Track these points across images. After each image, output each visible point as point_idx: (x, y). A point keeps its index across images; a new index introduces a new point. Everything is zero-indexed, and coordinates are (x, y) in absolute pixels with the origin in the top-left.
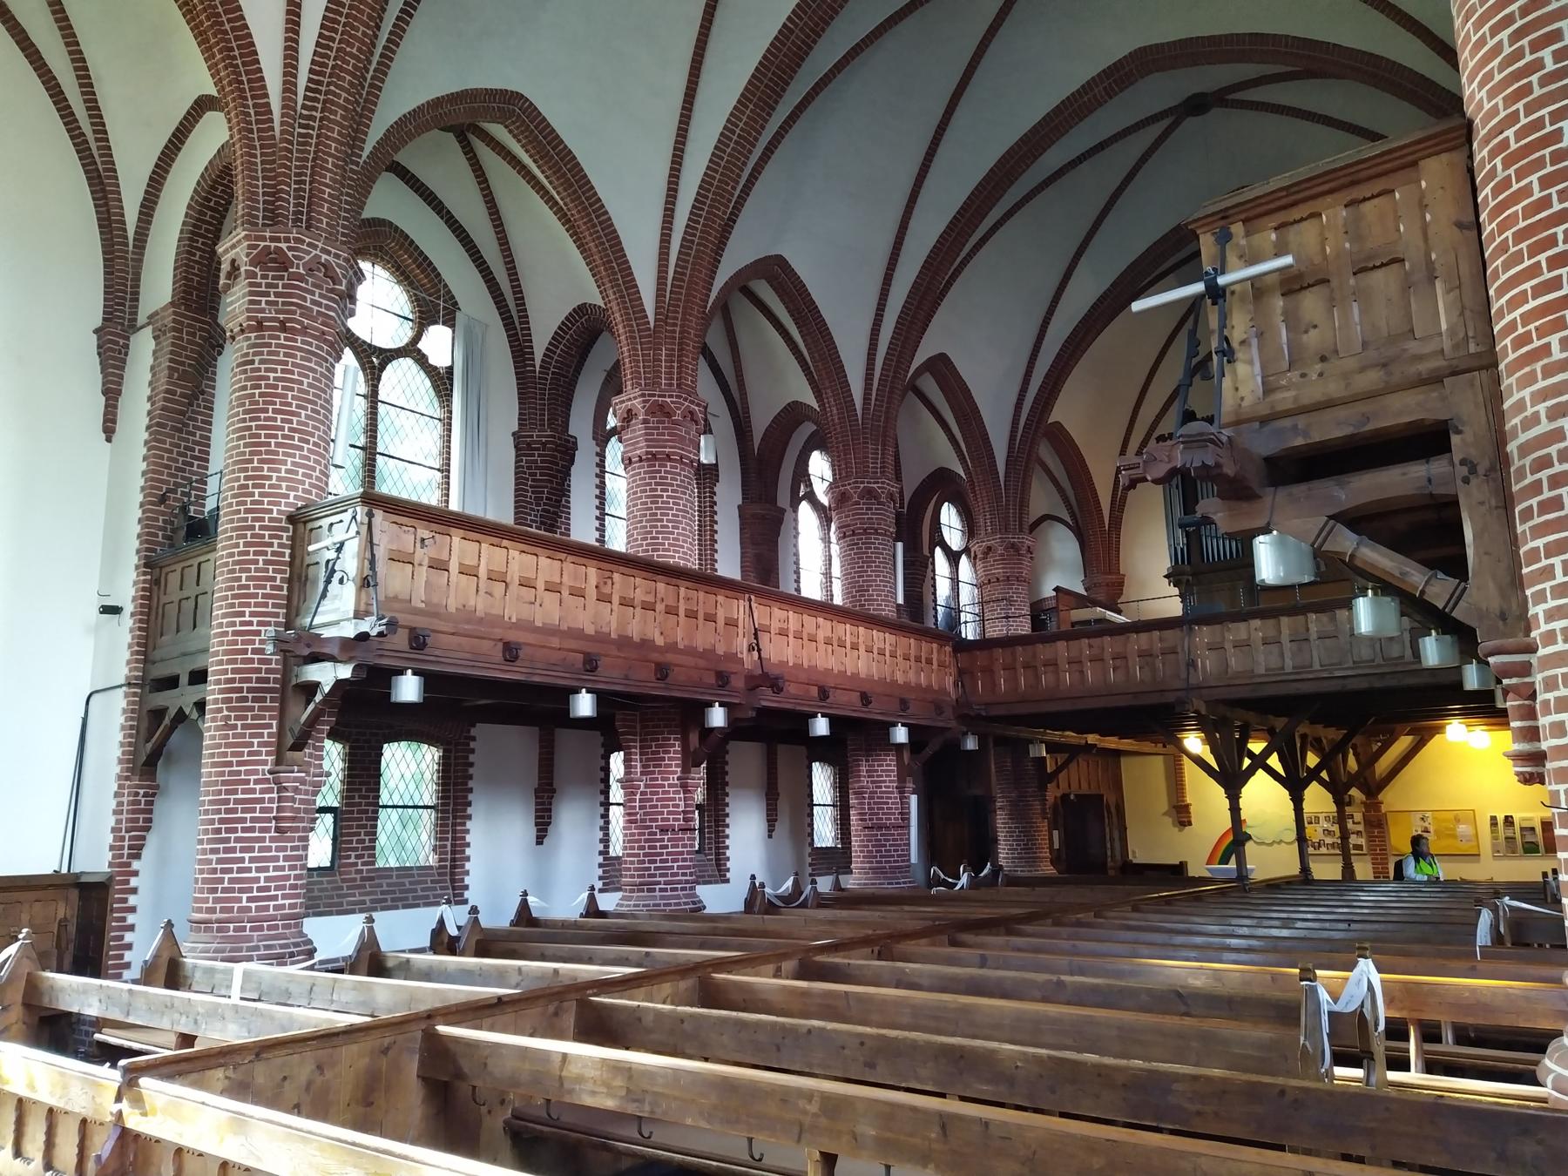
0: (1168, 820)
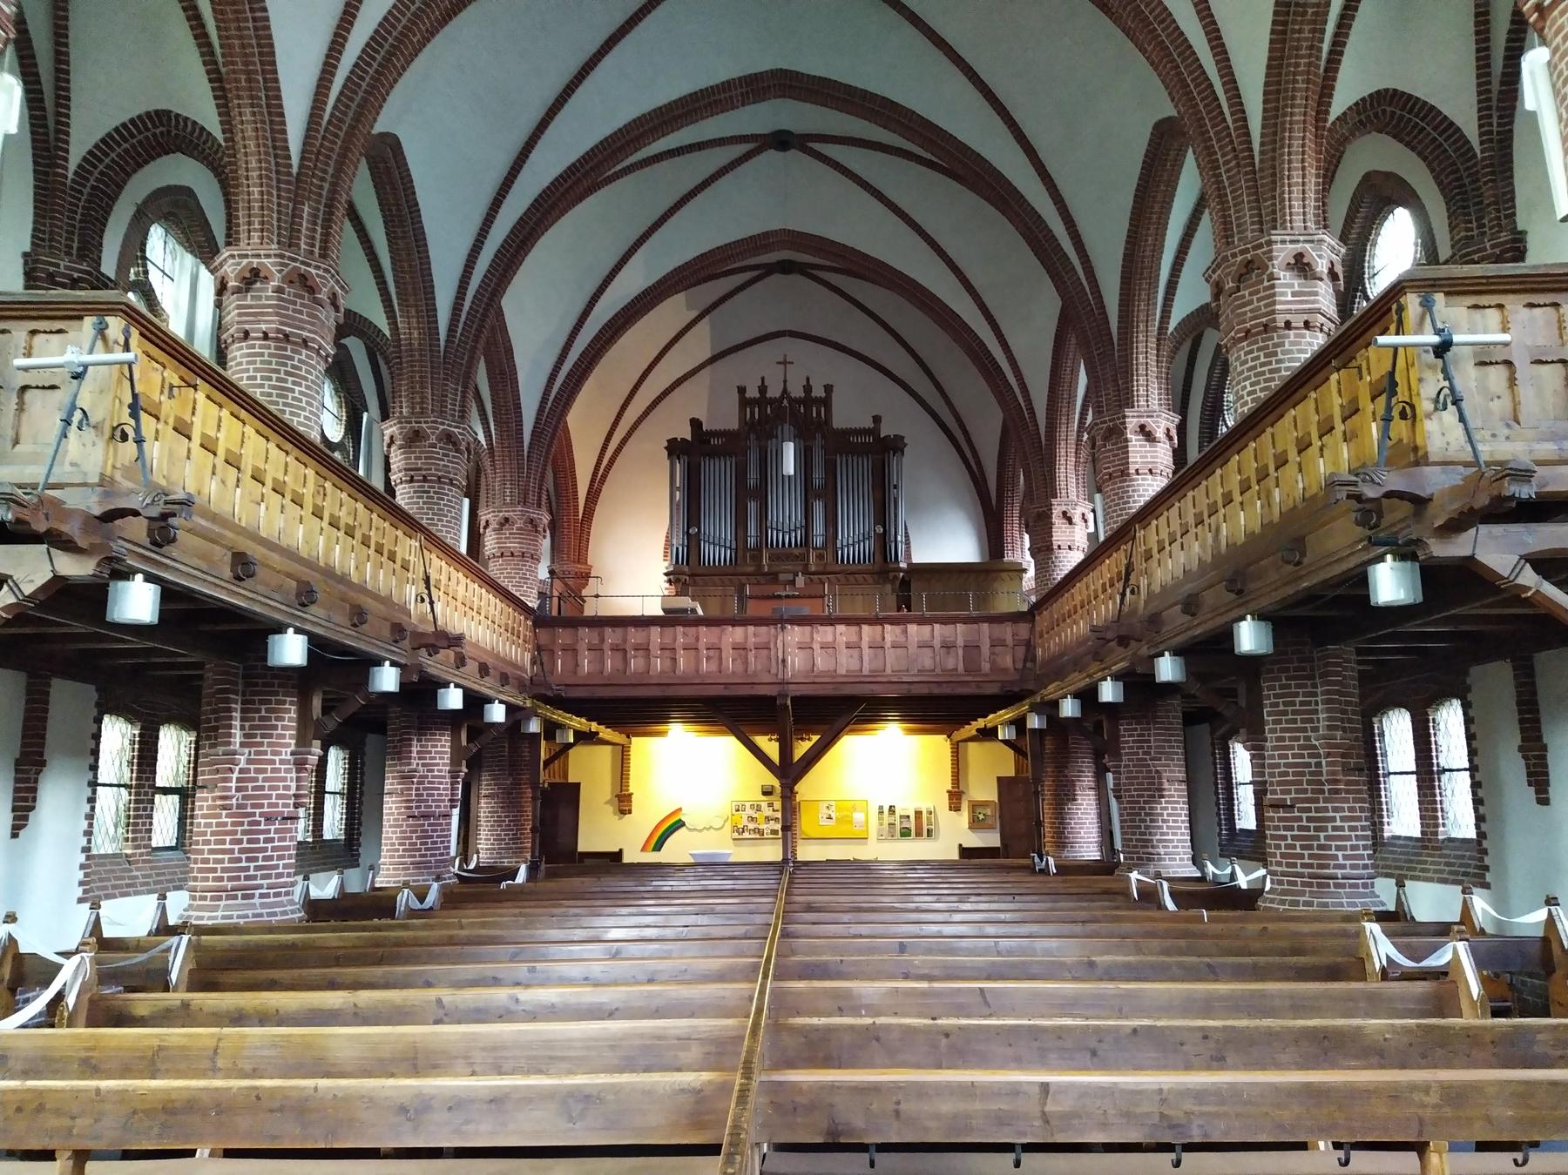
0: (610, 809)
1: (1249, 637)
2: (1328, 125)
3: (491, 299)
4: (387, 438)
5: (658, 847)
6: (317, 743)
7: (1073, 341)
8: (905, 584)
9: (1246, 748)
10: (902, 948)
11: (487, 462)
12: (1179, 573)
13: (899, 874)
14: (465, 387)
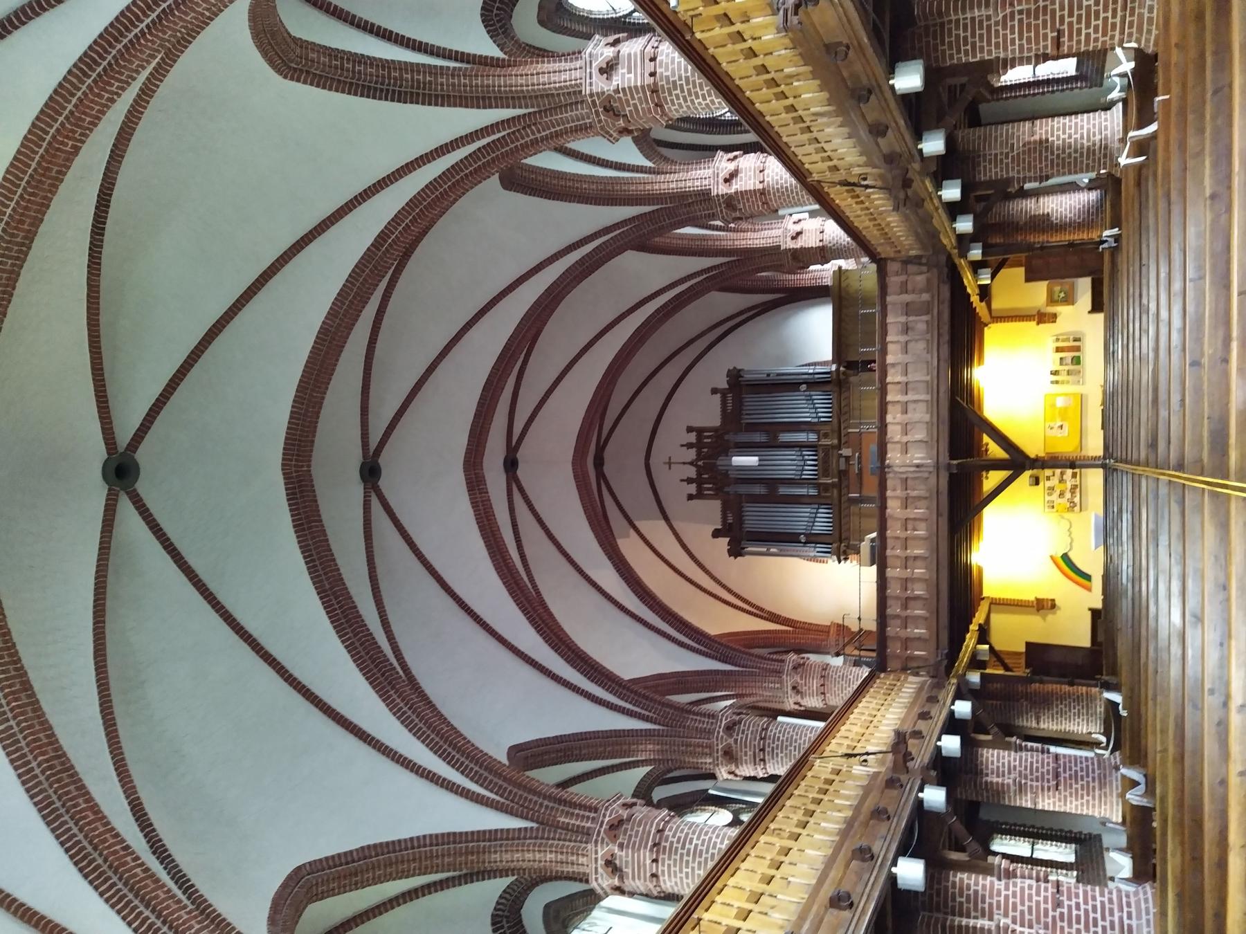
0: (1050, 617)
1: (909, 80)
2: (506, 57)
3: (624, 687)
4: (730, 777)
5: (1088, 577)
6: (990, 859)
7: (657, 239)
8: (851, 365)
9: (1005, 73)
10: (1196, 364)
11: (748, 700)
12: (850, 142)
13: (1118, 366)
14: (689, 712)
